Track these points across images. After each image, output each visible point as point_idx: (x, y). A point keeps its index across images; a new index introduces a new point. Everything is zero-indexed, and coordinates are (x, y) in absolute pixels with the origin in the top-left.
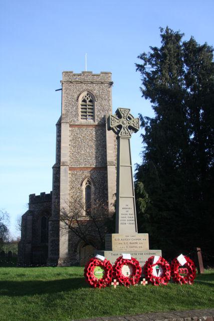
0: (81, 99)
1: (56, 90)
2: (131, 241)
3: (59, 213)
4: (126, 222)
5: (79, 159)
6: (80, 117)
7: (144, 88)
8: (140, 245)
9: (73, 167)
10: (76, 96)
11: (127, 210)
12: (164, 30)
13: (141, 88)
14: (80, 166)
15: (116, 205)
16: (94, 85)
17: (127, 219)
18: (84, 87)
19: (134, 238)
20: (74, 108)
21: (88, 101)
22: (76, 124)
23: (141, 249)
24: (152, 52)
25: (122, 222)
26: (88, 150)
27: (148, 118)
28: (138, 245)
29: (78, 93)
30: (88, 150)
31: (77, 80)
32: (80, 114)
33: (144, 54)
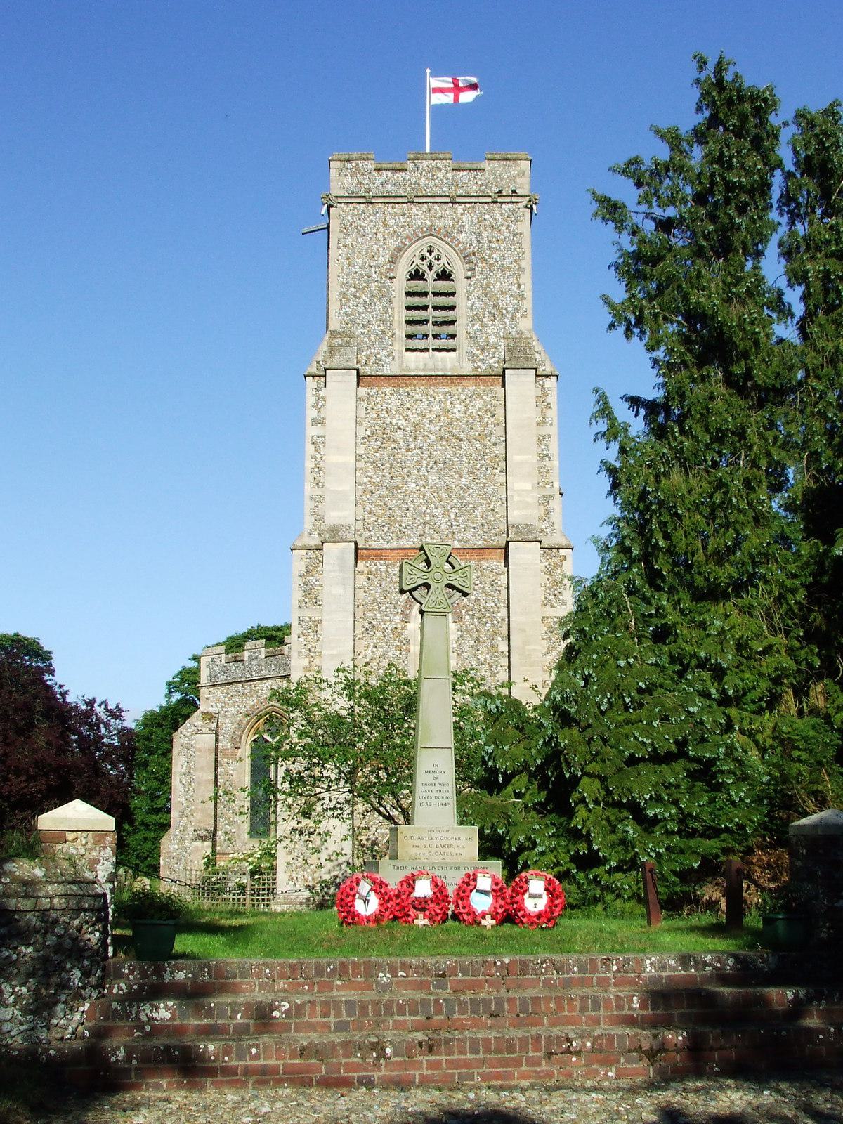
0: (403, 270)
1: (303, 234)
2: (440, 842)
3: (789, 856)
4: (433, 801)
5: (398, 513)
6: (399, 344)
7: (619, 293)
8: (458, 851)
9: (374, 544)
10: (383, 257)
11: (436, 775)
12: (711, 67)
13: (605, 298)
14: (402, 543)
15: (796, 702)
16: (460, 208)
17: (435, 793)
18: (419, 217)
19: (444, 835)
20: (379, 306)
21: (430, 275)
22: (387, 371)
23: (459, 860)
24: (664, 153)
25: (423, 801)
26: (432, 478)
27: (635, 401)
28: (455, 850)
29: (393, 244)
30: (432, 478)
31: (390, 188)
32: (401, 331)
33: (635, 161)
